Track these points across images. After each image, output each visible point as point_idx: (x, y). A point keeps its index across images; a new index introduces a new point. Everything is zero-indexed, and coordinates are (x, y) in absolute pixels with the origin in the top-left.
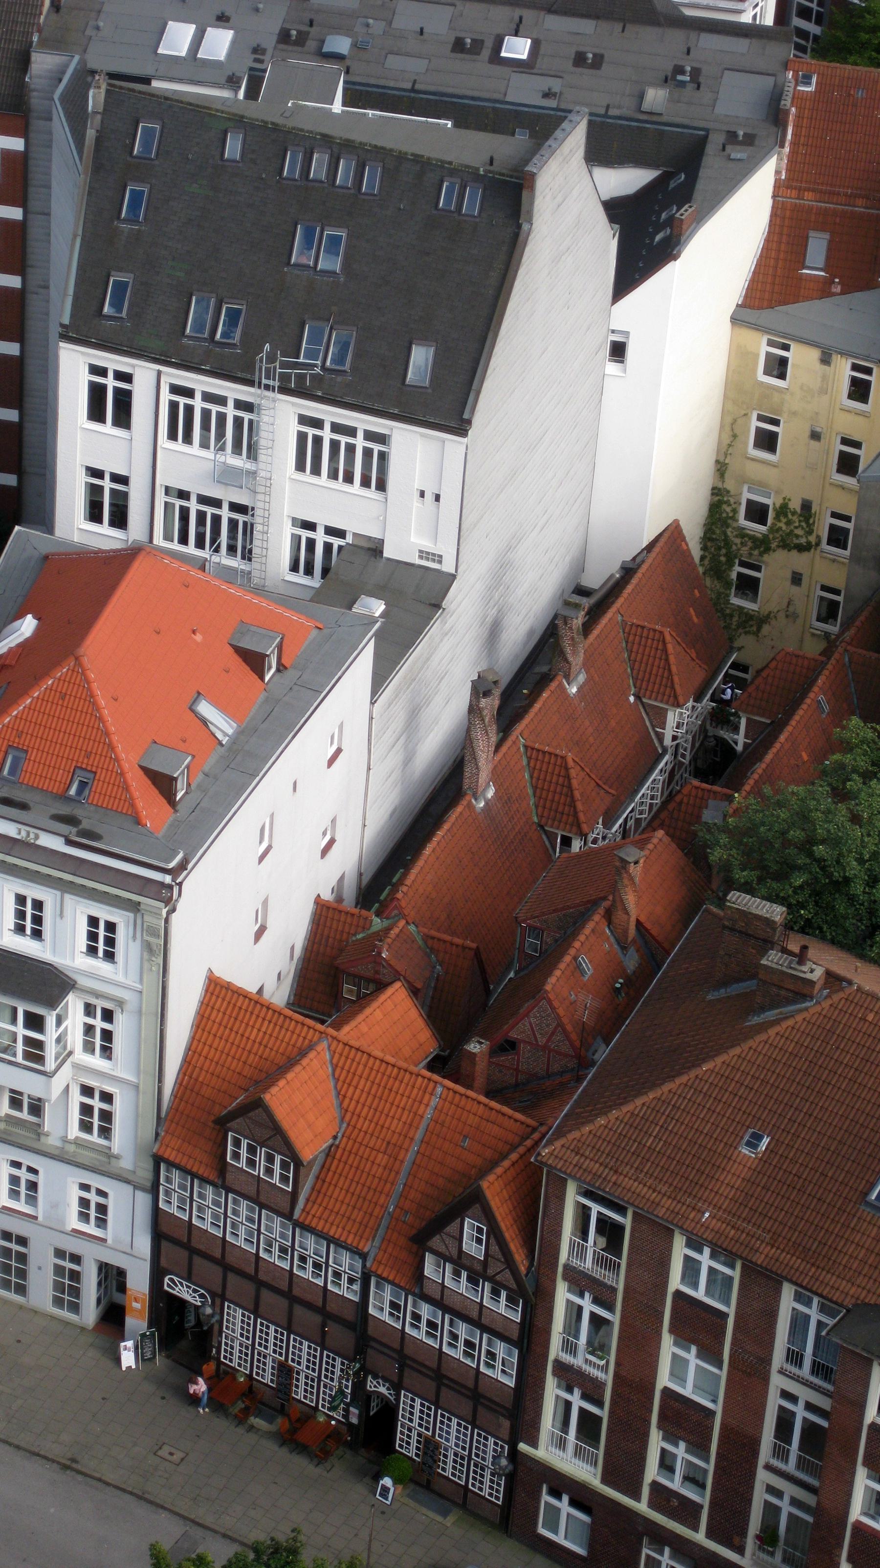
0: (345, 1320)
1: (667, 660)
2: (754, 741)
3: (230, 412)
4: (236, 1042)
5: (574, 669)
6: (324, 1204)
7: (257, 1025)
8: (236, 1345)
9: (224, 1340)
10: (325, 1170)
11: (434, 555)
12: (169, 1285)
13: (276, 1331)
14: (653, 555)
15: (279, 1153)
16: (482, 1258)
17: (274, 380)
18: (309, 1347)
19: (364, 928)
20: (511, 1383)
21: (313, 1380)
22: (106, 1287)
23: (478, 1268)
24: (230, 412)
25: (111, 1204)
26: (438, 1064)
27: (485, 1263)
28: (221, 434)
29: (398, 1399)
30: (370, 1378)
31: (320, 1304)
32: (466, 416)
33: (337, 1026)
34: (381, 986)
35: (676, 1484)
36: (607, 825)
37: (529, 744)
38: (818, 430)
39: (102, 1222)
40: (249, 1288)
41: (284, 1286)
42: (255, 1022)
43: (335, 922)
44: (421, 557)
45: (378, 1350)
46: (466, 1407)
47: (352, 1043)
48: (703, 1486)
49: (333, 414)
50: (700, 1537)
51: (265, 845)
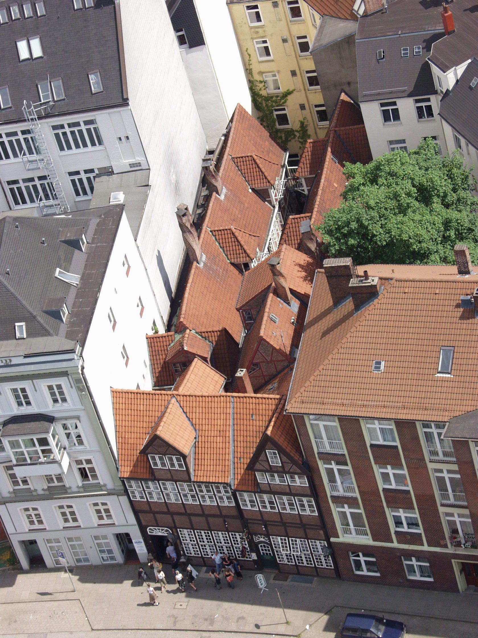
0: (232, 516)
1: (259, 167)
2: (311, 187)
3: (21, 137)
4: (136, 414)
5: (219, 188)
6: (203, 469)
7: (142, 403)
8: (190, 546)
9: (184, 546)
10: (197, 454)
11: (136, 164)
12: (150, 532)
13: (205, 533)
14: (234, 123)
15: (174, 455)
16: (281, 465)
17: (34, 115)
18: (222, 534)
19: (172, 341)
20: (316, 514)
21: (195, 545)
22: (123, 544)
23: (281, 470)
24: (21, 137)
25: (110, 507)
26: (227, 388)
27: (283, 467)
28: (21, 149)
29: (270, 541)
30: (254, 537)
31: (219, 513)
32: (125, 97)
33: (176, 389)
34: (190, 362)
35: (405, 529)
36: (262, 250)
37: (212, 229)
38: (285, 37)
39: (109, 517)
40: (186, 519)
41: (200, 512)
42: (140, 402)
43: (159, 343)
44: (131, 167)
45: (257, 524)
46: (301, 533)
47: (186, 393)
48: (417, 525)
49: (66, 120)
50: (426, 548)
51: (112, 322)
